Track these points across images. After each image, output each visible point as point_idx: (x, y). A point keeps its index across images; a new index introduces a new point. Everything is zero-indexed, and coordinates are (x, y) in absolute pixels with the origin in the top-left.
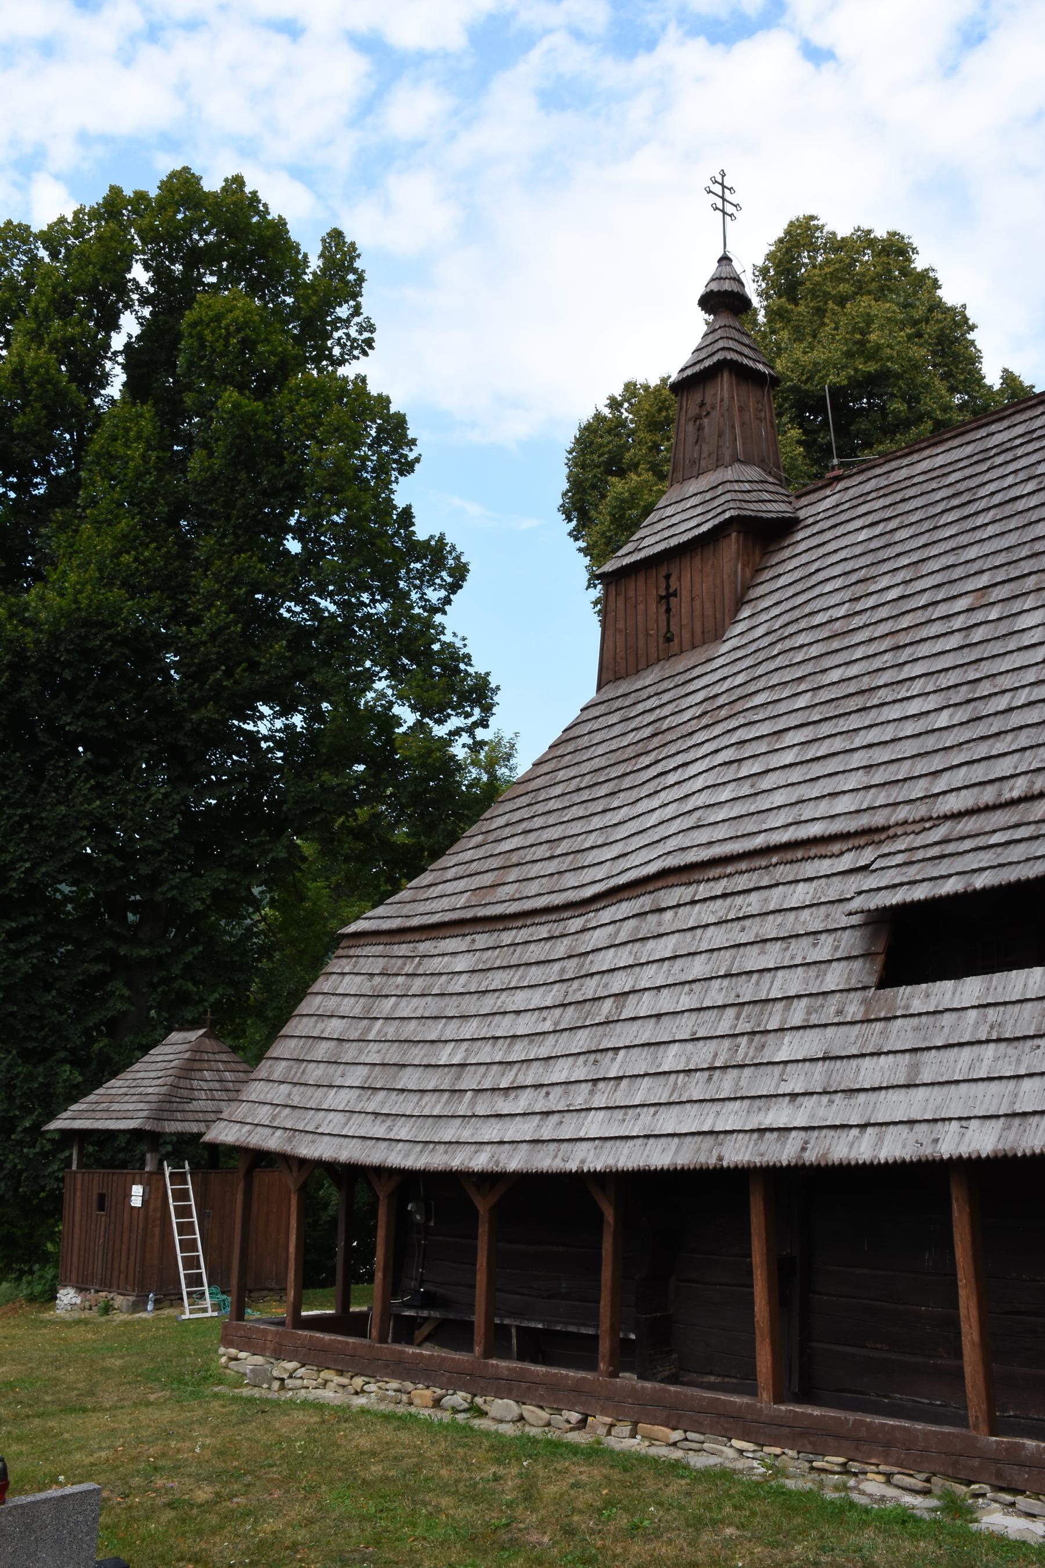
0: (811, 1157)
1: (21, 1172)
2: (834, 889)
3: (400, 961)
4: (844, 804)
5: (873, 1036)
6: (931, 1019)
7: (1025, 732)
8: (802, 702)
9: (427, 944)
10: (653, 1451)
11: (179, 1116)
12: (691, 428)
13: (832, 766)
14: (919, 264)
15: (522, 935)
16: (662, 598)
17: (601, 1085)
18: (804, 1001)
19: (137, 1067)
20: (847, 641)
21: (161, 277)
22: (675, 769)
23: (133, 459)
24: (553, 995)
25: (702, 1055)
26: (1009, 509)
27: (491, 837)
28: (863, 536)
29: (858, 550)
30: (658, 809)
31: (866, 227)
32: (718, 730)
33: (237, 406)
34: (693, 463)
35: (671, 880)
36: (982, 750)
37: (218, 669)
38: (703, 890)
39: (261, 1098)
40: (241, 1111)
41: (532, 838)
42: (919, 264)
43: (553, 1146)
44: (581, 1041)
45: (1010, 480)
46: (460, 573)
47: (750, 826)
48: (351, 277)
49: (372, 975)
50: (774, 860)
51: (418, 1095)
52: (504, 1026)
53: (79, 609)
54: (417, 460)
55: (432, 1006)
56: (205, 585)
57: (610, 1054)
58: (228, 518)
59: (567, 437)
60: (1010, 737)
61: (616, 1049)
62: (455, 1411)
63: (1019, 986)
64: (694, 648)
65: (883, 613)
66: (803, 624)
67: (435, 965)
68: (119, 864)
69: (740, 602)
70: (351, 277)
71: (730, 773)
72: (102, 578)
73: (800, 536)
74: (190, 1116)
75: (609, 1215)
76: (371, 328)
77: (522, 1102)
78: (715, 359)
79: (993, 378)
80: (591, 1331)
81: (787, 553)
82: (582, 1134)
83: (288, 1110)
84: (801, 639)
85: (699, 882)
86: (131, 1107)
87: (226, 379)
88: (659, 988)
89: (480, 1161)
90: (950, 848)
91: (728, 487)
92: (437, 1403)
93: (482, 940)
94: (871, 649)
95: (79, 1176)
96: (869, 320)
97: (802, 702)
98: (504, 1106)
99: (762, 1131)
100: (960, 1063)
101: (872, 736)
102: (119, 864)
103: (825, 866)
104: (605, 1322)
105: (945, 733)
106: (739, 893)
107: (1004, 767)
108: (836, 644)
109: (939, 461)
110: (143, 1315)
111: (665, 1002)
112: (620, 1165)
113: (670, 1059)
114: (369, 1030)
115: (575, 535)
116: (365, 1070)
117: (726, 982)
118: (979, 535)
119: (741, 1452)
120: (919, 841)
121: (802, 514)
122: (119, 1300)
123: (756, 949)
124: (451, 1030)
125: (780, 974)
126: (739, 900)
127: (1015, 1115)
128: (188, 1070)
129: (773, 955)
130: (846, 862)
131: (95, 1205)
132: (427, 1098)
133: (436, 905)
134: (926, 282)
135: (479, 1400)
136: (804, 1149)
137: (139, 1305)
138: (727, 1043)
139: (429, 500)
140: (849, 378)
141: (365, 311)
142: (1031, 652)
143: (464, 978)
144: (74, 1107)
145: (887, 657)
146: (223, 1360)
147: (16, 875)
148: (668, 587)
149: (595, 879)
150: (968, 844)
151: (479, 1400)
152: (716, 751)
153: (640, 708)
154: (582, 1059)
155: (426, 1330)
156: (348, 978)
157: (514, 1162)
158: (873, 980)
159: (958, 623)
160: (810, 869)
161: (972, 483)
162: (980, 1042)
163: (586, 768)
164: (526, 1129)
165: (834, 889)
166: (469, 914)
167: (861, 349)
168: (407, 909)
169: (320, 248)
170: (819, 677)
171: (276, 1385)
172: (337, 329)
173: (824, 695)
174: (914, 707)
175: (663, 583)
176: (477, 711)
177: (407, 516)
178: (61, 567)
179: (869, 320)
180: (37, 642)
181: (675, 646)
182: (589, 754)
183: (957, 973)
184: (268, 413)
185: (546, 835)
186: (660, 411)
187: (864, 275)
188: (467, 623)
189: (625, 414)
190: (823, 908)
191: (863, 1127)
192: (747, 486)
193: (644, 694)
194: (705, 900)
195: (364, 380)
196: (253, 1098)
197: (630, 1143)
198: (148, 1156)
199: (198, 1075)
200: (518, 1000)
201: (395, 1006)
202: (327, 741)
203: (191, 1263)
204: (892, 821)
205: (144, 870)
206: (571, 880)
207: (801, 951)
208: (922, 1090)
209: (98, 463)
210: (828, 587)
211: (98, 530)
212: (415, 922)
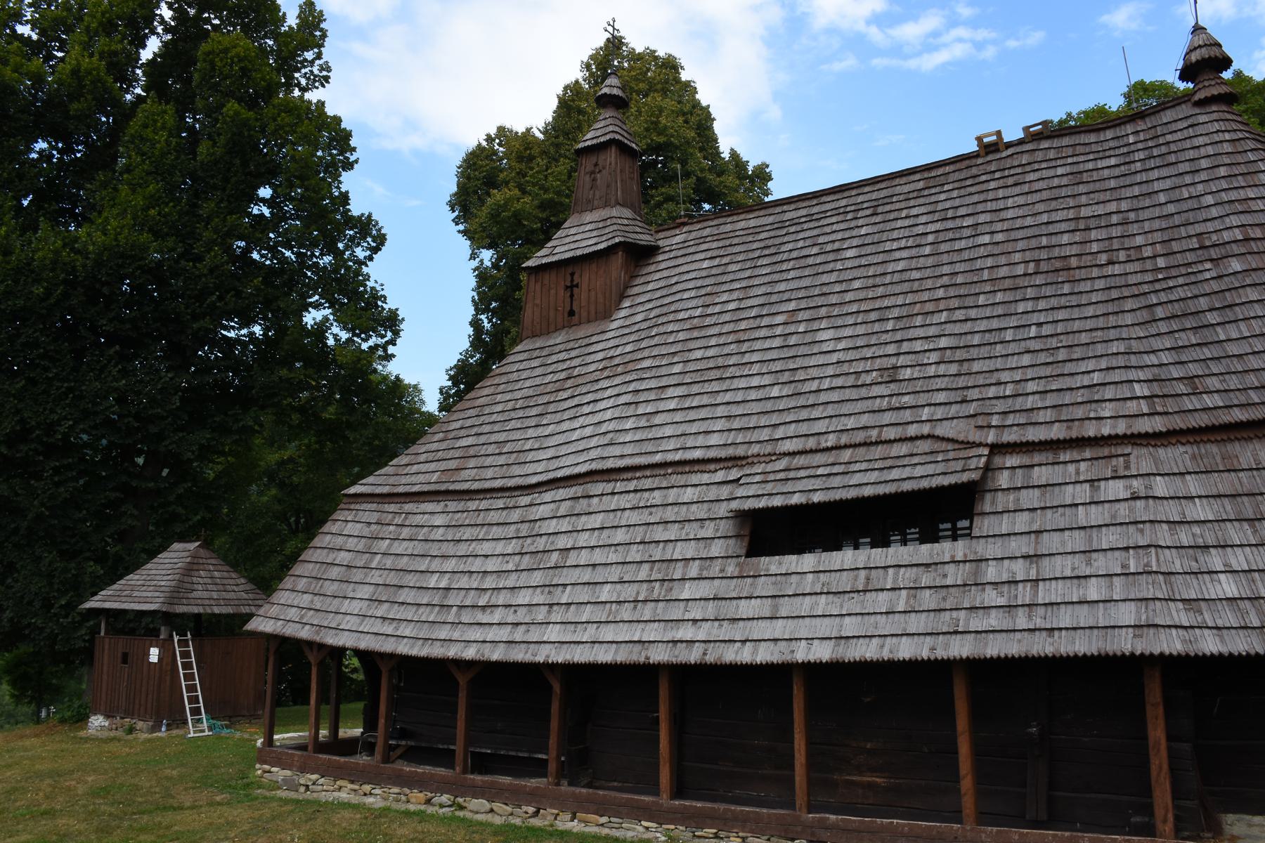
0: (710, 659)
1: (57, 635)
2: (713, 493)
3: (390, 516)
4: (714, 440)
5: (746, 586)
6: (783, 578)
7: (830, 406)
8: (677, 369)
9: (411, 505)
10: (587, 829)
11: (184, 601)
12: (587, 178)
13: (703, 413)
14: (684, 76)
15: (484, 504)
16: (567, 287)
17: (555, 608)
18: (697, 562)
19: (149, 566)
20: (703, 333)
21: (180, 15)
22: (588, 403)
23: (159, 142)
24: (511, 547)
25: (629, 592)
26: (803, 262)
27: (452, 435)
28: (706, 264)
29: (704, 273)
30: (580, 428)
31: (652, 48)
32: (617, 380)
33: (237, 113)
34: (589, 201)
35: (596, 478)
36: (804, 414)
37: (213, 294)
38: (619, 486)
39: (289, 602)
40: (274, 611)
41: (482, 439)
42: (684, 76)
43: (523, 646)
44: (537, 578)
45: (801, 244)
46: (381, 240)
47: (650, 447)
48: (318, 33)
49: (369, 523)
50: (670, 471)
51: (415, 608)
52: (477, 565)
53: (118, 246)
54: (356, 161)
55: (419, 548)
56: (207, 235)
57: (560, 588)
58: (224, 190)
59: (458, 158)
60: (821, 408)
61: (565, 585)
62: (442, 806)
63: (839, 562)
64: (589, 322)
65: (727, 317)
66: (671, 317)
67: (419, 519)
68: (136, 425)
69: (622, 297)
70: (318, 33)
71: (630, 411)
72: (134, 225)
73: (660, 258)
74: (192, 601)
75: (557, 687)
76: (329, 69)
77: (497, 616)
78: (608, 137)
79: (726, 155)
80: (544, 757)
81: (652, 268)
82: (545, 639)
83: (312, 612)
84: (670, 328)
85: (616, 481)
86: (149, 594)
87: (229, 94)
88: (592, 548)
89: (470, 653)
90: (792, 474)
91: (614, 221)
92: (428, 802)
93: (452, 506)
94: (722, 340)
95: (107, 640)
96: (661, 110)
97: (677, 369)
98: (485, 618)
99: (675, 642)
100: (805, 605)
101: (728, 397)
102: (136, 425)
103: (706, 478)
104: (553, 753)
105: (778, 401)
106: (646, 490)
107: (820, 426)
108: (696, 334)
109: (752, 223)
110: (159, 734)
111: (598, 556)
112: (576, 660)
113: (605, 593)
114: (371, 561)
115: (456, 221)
116: (372, 588)
117: (641, 547)
118: (785, 276)
119: (647, 828)
120: (769, 468)
121: (661, 243)
122: (140, 724)
123: (661, 527)
124: (435, 565)
125: (679, 544)
126: (646, 495)
127: (842, 638)
128: (189, 570)
129: (672, 532)
130: (720, 476)
131: (120, 660)
132: (422, 609)
133: (414, 479)
134: (689, 88)
135: (460, 800)
136: (705, 654)
137: (156, 728)
138: (645, 586)
139: (362, 190)
140: (648, 145)
141: (325, 58)
142: (828, 356)
143: (441, 530)
144: (103, 593)
145: (733, 346)
146: (259, 772)
147: (62, 429)
148: (572, 281)
149: (537, 471)
150: (802, 473)
151: (460, 800)
152: (618, 395)
153: (554, 358)
154: (539, 590)
155: (399, 752)
156: (350, 525)
157: (496, 655)
158: (743, 552)
159: (779, 331)
160: (695, 479)
161: (777, 241)
162: (816, 594)
163: (518, 395)
164: (503, 634)
165: (713, 493)
166: (443, 487)
167: (654, 126)
168: (392, 480)
169: (297, 12)
170: (687, 354)
171: (302, 789)
172: (305, 67)
173: (691, 367)
174: (755, 381)
175: (569, 278)
176: (389, 334)
177: (345, 198)
178: (105, 214)
179: (661, 110)
180: (84, 266)
181: (575, 319)
182: (519, 385)
183: (800, 551)
184: (257, 120)
185: (494, 438)
186: (526, 149)
187: (654, 79)
188: (384, 273)
189: (497, 147)
190: (705, 505)
191: (744, 642)
192: (626, 222)
193: (557, 349)
194: (621, 493)
195: (323, 103)
196: (282, 601)
197: (581, 646)
198: (163, 628)
199: (196, 573)
200: (486, 548)
201: (390, 546)
202: (286, 347)
203: (193, 700)
204: (750, 453)
205: (153, 429)
206: (517, 470)
207: (692, 530)
208: (780, 621)
209: (132, 143)
210: (686, 295)
211: (134, 191)
212: (401, 490)
